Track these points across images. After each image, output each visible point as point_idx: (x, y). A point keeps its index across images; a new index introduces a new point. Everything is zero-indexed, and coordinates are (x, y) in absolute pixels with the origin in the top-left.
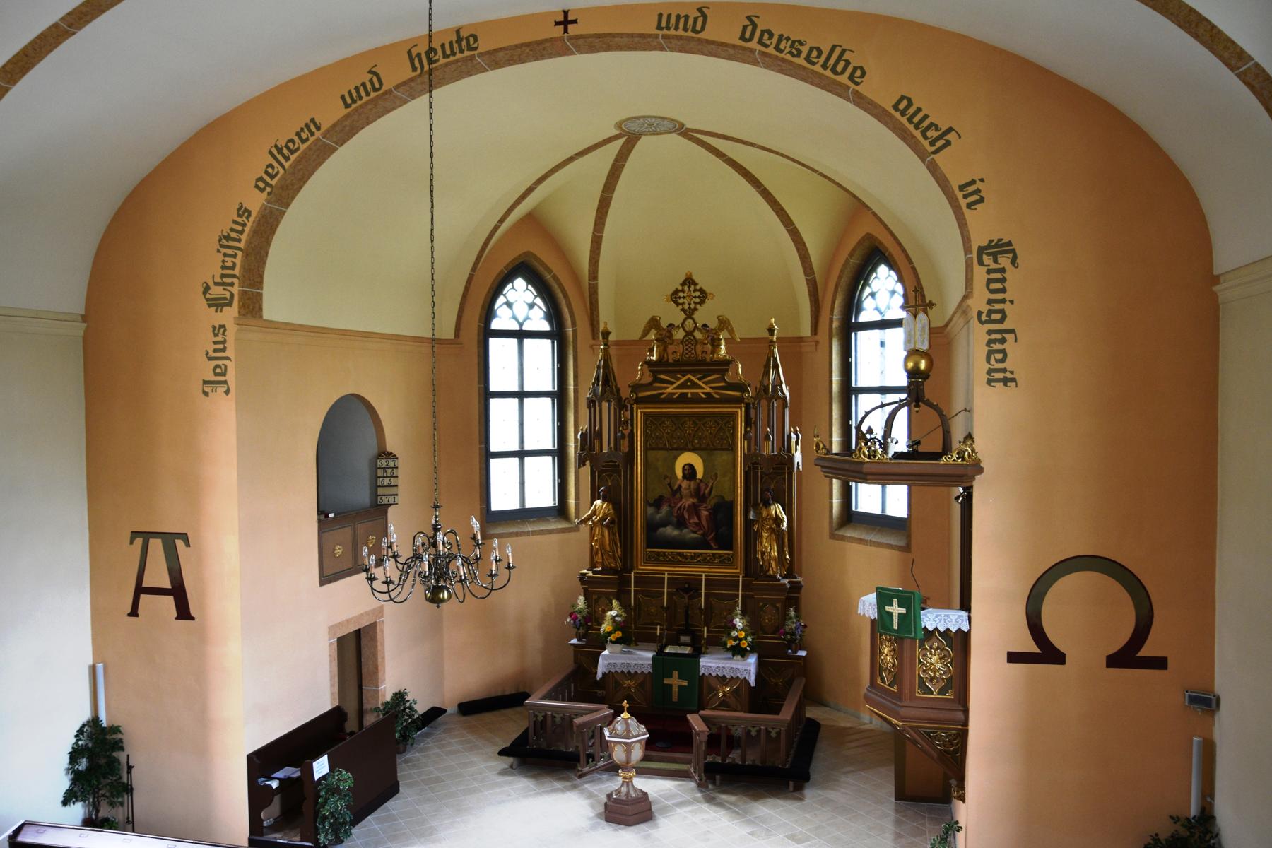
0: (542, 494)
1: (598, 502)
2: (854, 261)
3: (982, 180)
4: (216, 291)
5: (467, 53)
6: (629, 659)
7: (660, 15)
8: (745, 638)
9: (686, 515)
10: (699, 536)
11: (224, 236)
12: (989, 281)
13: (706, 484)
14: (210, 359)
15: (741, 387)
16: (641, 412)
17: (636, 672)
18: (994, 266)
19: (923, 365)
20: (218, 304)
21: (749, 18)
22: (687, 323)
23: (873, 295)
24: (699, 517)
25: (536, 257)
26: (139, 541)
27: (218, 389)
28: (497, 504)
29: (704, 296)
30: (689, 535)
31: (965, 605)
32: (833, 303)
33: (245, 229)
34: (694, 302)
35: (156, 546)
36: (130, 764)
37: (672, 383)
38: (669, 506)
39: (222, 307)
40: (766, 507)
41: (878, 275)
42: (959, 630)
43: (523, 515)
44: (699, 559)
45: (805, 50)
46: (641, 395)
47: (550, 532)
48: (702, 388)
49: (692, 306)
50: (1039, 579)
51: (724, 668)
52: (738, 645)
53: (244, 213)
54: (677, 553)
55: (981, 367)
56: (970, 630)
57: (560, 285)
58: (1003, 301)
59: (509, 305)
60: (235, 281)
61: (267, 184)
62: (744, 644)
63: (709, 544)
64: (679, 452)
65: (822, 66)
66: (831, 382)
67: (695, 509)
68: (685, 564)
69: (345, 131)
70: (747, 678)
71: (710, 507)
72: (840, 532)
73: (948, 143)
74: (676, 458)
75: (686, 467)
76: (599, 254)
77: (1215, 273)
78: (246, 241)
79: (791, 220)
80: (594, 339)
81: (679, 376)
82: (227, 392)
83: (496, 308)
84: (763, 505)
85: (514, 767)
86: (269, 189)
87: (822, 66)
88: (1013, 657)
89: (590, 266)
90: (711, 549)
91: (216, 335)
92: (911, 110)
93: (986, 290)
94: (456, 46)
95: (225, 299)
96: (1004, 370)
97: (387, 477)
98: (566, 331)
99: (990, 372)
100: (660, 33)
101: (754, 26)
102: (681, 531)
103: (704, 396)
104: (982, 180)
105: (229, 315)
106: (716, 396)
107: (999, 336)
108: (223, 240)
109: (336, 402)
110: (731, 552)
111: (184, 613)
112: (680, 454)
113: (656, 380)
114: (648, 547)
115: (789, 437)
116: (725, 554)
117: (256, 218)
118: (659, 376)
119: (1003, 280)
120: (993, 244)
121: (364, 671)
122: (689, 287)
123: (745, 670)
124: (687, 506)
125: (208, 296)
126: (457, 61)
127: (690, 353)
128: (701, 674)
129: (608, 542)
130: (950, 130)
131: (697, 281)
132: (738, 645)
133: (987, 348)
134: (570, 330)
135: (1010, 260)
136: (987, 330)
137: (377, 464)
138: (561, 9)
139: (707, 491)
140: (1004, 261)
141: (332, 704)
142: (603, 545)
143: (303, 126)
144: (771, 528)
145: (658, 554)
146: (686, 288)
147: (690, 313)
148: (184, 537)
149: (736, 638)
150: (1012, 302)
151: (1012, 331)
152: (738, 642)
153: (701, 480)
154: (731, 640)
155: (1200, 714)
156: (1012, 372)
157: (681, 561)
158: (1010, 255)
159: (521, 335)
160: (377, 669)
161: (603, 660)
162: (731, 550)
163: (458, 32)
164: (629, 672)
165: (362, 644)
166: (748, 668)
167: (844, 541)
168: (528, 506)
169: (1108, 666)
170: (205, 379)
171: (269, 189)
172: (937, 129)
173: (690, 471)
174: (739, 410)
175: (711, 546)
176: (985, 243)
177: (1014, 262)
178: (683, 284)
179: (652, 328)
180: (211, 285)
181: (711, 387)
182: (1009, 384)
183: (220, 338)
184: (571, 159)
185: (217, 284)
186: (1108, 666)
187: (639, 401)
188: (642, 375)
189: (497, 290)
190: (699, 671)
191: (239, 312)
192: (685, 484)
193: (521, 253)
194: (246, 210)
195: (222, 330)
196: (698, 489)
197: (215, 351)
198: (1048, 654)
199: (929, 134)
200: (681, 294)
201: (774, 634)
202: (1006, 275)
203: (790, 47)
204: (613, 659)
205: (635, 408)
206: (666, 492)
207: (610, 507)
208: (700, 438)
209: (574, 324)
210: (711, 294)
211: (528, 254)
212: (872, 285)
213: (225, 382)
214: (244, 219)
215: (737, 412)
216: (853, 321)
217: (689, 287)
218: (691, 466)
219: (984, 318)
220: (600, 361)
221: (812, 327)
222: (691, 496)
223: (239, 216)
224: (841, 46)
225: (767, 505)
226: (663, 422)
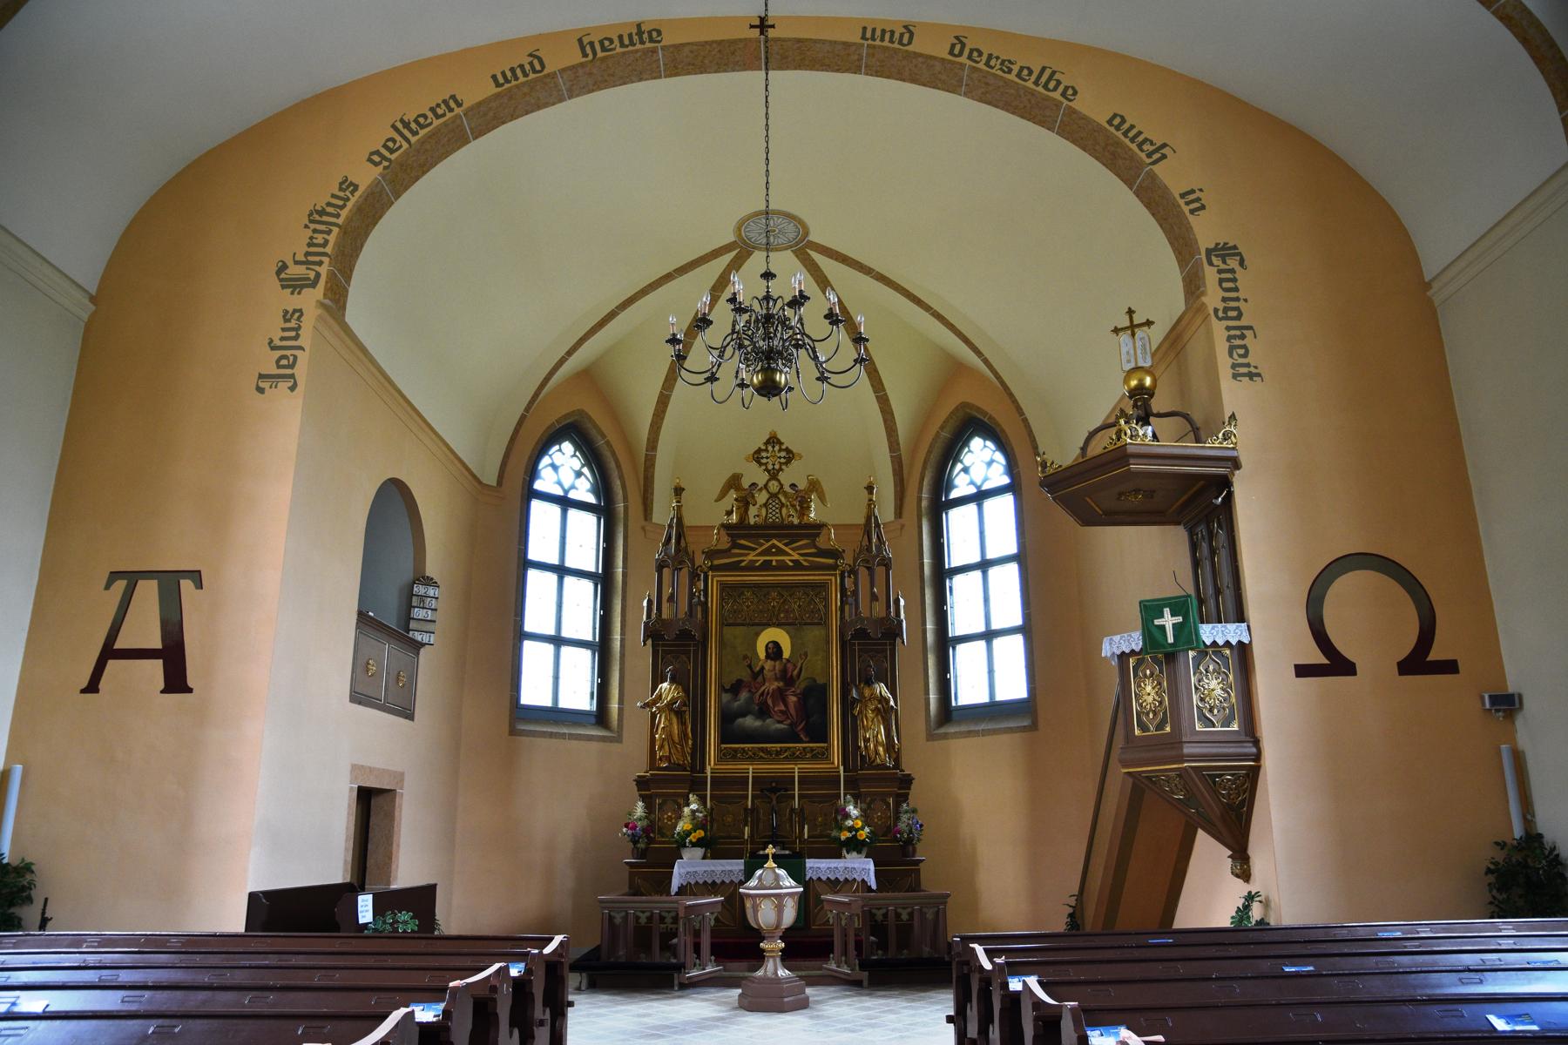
0: (578, 694)
1: (665, 685)
2: (946, 434)
3: (1201, 190)
4: (295, 271)
5: (648, 45)
6: (714, 866)
7: (865, 29)
8: (862, 828)
9: (770, 702)
10: (785, 726)
11: (315, 210)
12: (1221, 281)
13: (794, 665)
14: (274, 348)
15: (835, 554)
16: (717, 581)
17: (723, 882)
18: (1223, 267)
19: (1148, 381)
20: (296, 285)
21: (957, 38)
22: (771, 484)
23: (966, 470)
24: (786, 705)
25: (590, 418)
26: (121, 585)
27: (279, 384)
28: (527, 698)
29: (790, 456)
30: (773, 725)
31: (1240, 617)
32: (922, 479)
33: (347, 203)
34: (779, 462)
35: (148, 593)
36: (48, 915)
37: (754, 549)
38: (750, 691)
39: (301, 289)
40: (869, 685)
41: (971, 449)
42: (1240, 642)
43: (554, 715)
44: (786, 754)
45: (1016, 69)
46: (716, 562)
47: (590, 738)
48: (789, 555)
49: (777, 467)
50: (1315, 581)
51: (837, 868)
52: (855, 836)
53: (348, 187)
54: (759, 749)
55: (1224, 363)
56: (1251, 642)
57: (614, 454)
58: (1237, 299)
59: (555, 467)
60: (326, 260)
61: (384, 158)
62: (861, 835)
63: (798, 736)
64: (762, 627)
65: (1034, 83)
66: (922, 565)
67: (780, 695)
68: (773, 761)
69: (489, 117)
70: (866, 879)
71: (798, 691)
72: (942, 730)
73: (1164, 157)
74: (758, 634)
75: (770, 645)
76: (663, 419)
77: (1426, 280)
78: (347, 217)
79: (883, 385)
80: (646, 520)
81: (762, 541)
82: (292, 388)
83: (540, 467)
84: (865, 684)
85: (583, 988)
86: (386, 164)
87: (1034, 83)
88: (1302, 671)
89: (649, 434)
90: (801, 741)
91: (287, 321)
92: (1126, 126)
93: (1219, 288)
94: (636, 38)
95: (309, 279)
96: (1248, 365)
97: (423, 608)
98: (614, 509)
99: (1234, 366)
100: (866, 43)
101: (963, 45)
102: (764, 721)
103: (791, 564)
104: (1201, 190)
105: (310, 300)
106: (805, 564)
107: (1238, 333)
108: (315, 215)
109: (380, 488)
110: (826, 745)
111: (176, 682)
112: (762, 631)
113: (735, 545)
114: (723, 743)
115: (897, 602)
116: (818, 747)
117: (363, 192)
118: (738, 541)
119: (1234, 280)
120: (1220, 246)
121: (370, 862)
122: (773, 447)
123: (863, 869)
124: (771, 691)
125: (283, 276)
126: (637, 51)
127: (774, 518)
128: (807, 879)
129: (676, 732)
130: (1164, 145)
131: (782, 440)
132: (855, 836)
133: (1228, 344)
134: (620, 506)
135: (1237, 262)
136: (1225, 326)
137: (413, 590)
138: (757, 15)
139: (795, 672)
140: (1233, 263)
141: (344, 879)
142: (671, 735)
143: (440, 102)
144: (877, 708)
145: (736, 750)
146: (770, 448)
147: (774, 475)
148: (196, 577)
149: (850, 829)
150: (1246, 300)
151: (1250, 328)
152: (854, 833)
153: (788, 660)
154: (845, 832)
155: (1501, 719)
156: (1256, 367)
157: (764, 758)
158: (1238, 258)
159: (565, 503)
160: (390, 858)
161: (679, 868)
162: (825, 742)
163: (639, 26)
164: (714, 882)
165: (371, 824)
166: (867, 867)
167: (948, 739)
168: (563, 704)
169: (1401, 673)
170: (262, 373)
171: (386, 164)
172: (1152, 143)
173: (774, 651)
174: (833, 578)
175: (801, 739)
176: (1212, 246)
177: (1242, 263)
178: (767, 443)
179: (731, 487)
180: (290, 263)
181: (798, 554)
182: (1255, 379)
183: (293, 324)
184: (668, 278)
185: (297, 263)
186: (1401, 673)
187: (713, 568)
188: (718, 540)
189: (542, 449)
190: (805, 875)
191: (325, 295)
192: (769, 665)
193: (575, 409)
194: (351, 184)
195: (297, 315)
196: (784, 670)
197: (282, 339)
198: (1338, 665)
199: (1145, 147)
200: (764, 454)
201: (886, 836)
202: (1236, 276)
203: (1001, 65)
204: (693, 867)
205: (710, 577)
206: (744, 674)
207: (680, 689)
208: (787, 611)
209: (625, 499)
210: (799, 454)
211: (581, 412)
212: (964, 461)
213: (292, 376)
214: (348, 193)
215: (831, 580)
216: (943, 499)
217: (773, 447)
218: (776, 645)
219: (1220, 314)
220: (672, 519)
221: (896, 509)
222: (777, 679)
223: (341, 189)
224: (1050, 68)
225: (869, 683)
226: (742, 593)
